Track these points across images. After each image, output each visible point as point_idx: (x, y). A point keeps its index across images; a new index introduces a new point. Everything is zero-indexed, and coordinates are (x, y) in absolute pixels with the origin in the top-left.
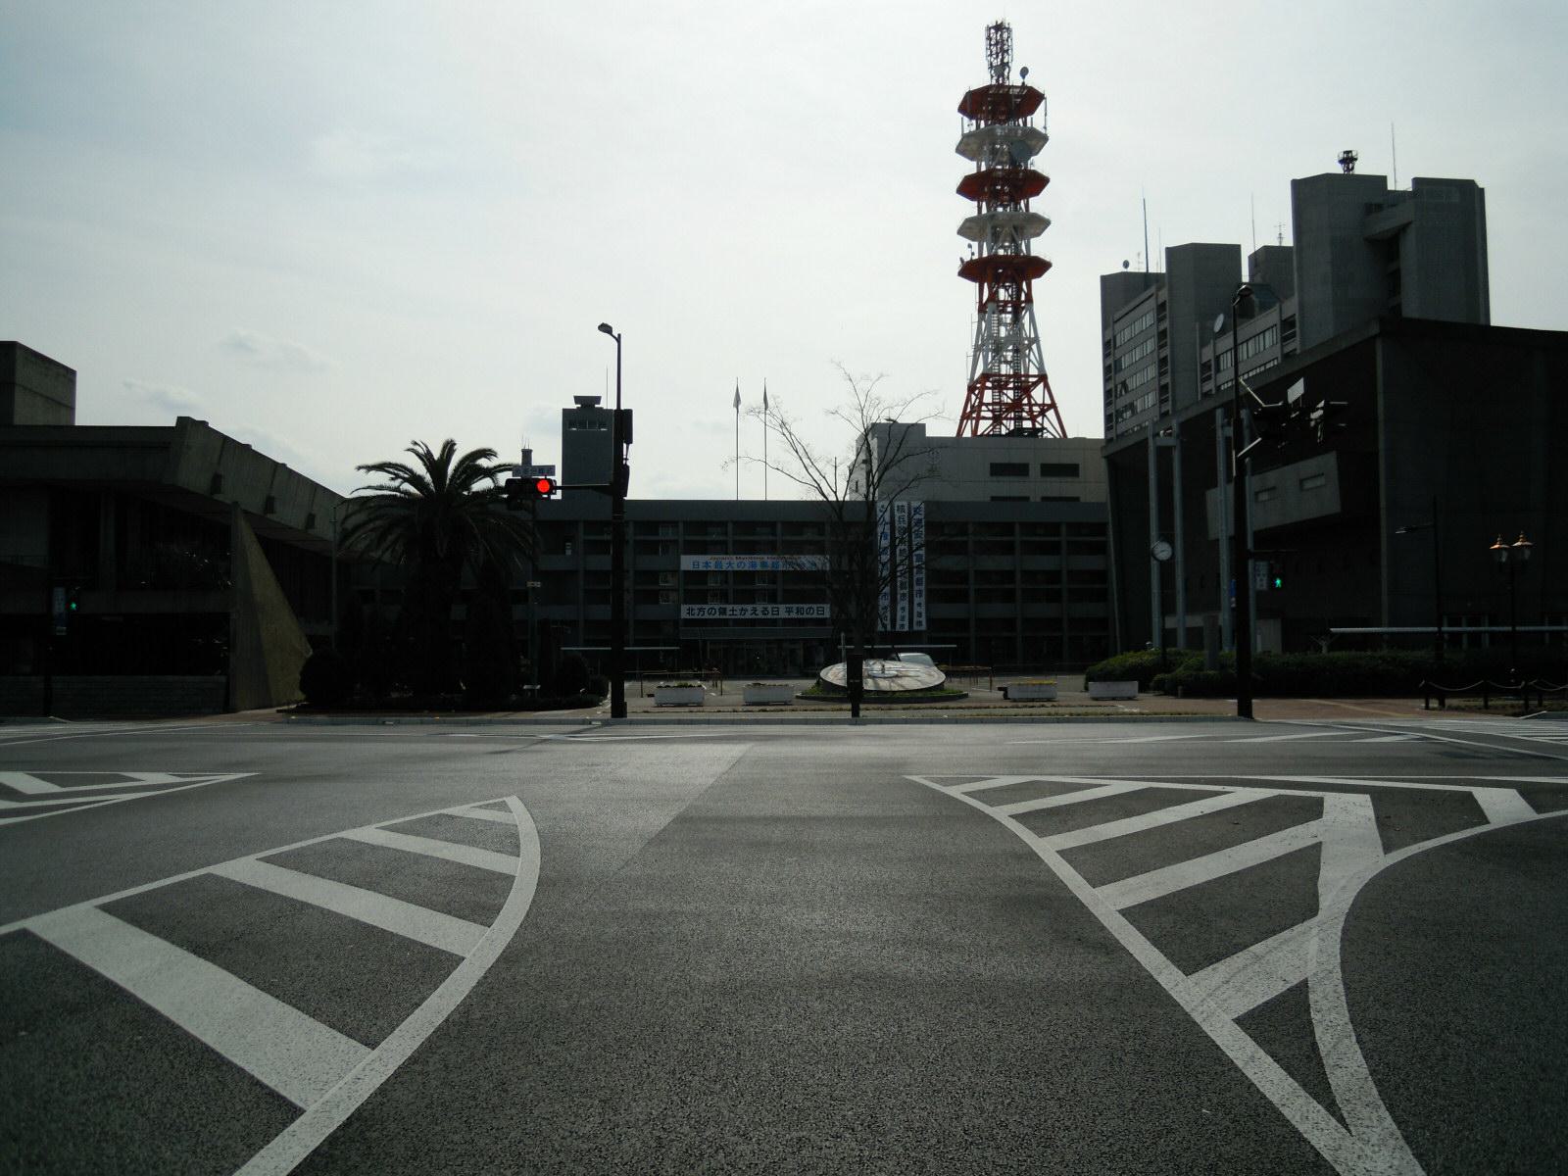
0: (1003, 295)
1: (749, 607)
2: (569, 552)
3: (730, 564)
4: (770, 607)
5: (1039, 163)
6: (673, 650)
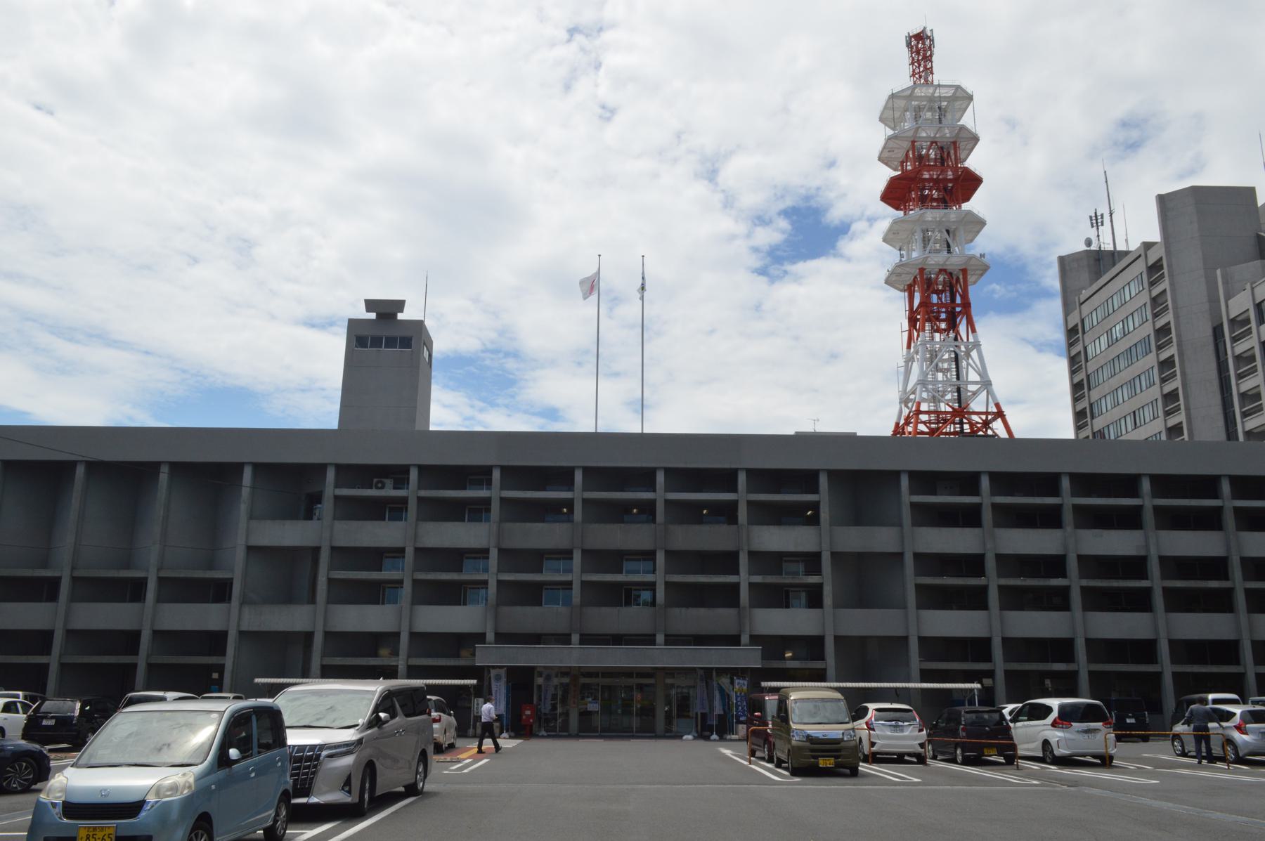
5: (974, 162)
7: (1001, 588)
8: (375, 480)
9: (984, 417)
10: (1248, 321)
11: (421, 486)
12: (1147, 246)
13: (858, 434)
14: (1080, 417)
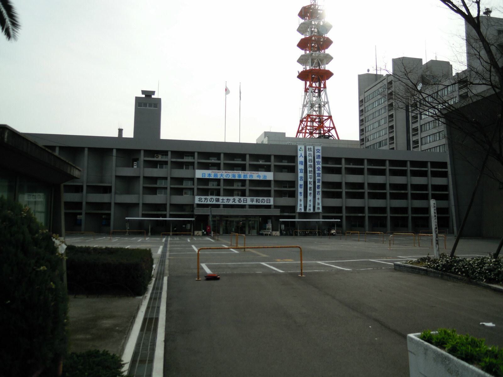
0: (314, 85)
1: (231, 198)
2: (135, 167)
3: (222, 175)
4: (242, 198)
5: (329, 35)
6: (191, 220)
8: (155, 155)
9: (328, 128)
11: (172, 158)
13: (287, 136)
14: (362, 131)
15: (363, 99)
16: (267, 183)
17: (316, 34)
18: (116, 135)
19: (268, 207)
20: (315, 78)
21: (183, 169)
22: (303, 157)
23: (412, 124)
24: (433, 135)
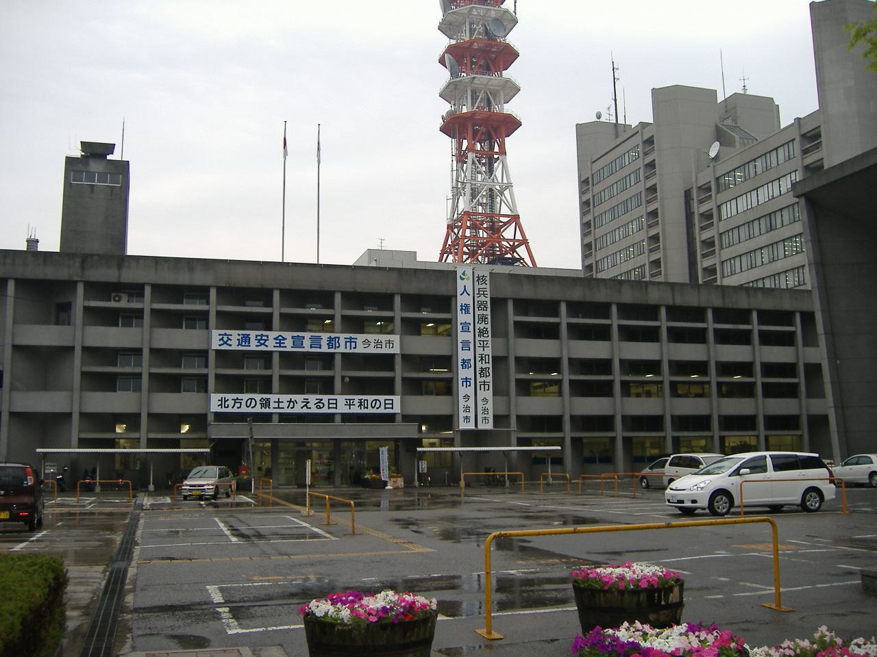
1: (299, 398)
4: (325, 398)
7: (571, 381)
8: (113, 294)
10: (709, 189)
11: (152, 301)
12: (643, 125)
14: (587, 248)
15: (588, 178)
16: (386, 361)
17: (481, 37)
18: (23, 247)
19: (390, 418)
20: (480, 133)
21: (182, 328)
22: (469, 295)
23: (699, 232)
24: (770, 248)
